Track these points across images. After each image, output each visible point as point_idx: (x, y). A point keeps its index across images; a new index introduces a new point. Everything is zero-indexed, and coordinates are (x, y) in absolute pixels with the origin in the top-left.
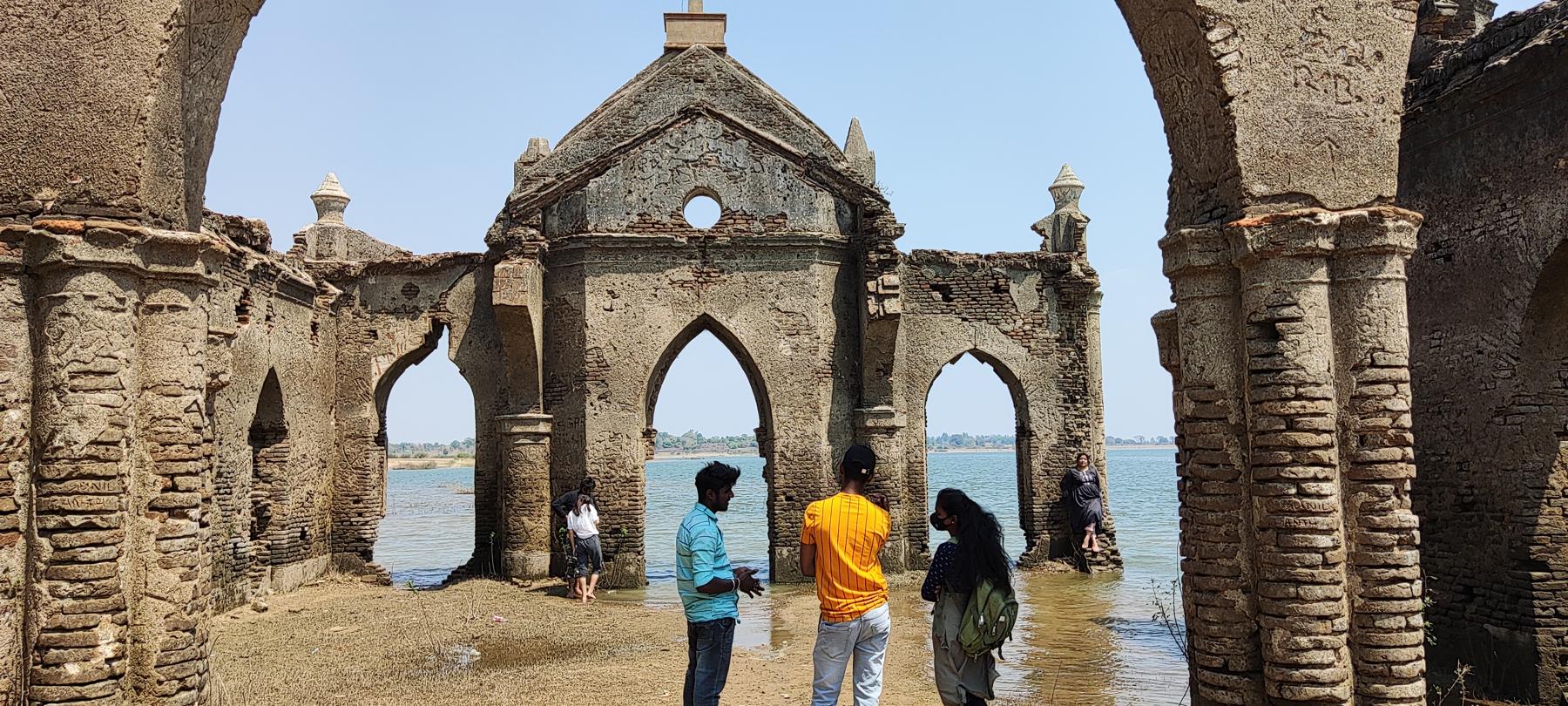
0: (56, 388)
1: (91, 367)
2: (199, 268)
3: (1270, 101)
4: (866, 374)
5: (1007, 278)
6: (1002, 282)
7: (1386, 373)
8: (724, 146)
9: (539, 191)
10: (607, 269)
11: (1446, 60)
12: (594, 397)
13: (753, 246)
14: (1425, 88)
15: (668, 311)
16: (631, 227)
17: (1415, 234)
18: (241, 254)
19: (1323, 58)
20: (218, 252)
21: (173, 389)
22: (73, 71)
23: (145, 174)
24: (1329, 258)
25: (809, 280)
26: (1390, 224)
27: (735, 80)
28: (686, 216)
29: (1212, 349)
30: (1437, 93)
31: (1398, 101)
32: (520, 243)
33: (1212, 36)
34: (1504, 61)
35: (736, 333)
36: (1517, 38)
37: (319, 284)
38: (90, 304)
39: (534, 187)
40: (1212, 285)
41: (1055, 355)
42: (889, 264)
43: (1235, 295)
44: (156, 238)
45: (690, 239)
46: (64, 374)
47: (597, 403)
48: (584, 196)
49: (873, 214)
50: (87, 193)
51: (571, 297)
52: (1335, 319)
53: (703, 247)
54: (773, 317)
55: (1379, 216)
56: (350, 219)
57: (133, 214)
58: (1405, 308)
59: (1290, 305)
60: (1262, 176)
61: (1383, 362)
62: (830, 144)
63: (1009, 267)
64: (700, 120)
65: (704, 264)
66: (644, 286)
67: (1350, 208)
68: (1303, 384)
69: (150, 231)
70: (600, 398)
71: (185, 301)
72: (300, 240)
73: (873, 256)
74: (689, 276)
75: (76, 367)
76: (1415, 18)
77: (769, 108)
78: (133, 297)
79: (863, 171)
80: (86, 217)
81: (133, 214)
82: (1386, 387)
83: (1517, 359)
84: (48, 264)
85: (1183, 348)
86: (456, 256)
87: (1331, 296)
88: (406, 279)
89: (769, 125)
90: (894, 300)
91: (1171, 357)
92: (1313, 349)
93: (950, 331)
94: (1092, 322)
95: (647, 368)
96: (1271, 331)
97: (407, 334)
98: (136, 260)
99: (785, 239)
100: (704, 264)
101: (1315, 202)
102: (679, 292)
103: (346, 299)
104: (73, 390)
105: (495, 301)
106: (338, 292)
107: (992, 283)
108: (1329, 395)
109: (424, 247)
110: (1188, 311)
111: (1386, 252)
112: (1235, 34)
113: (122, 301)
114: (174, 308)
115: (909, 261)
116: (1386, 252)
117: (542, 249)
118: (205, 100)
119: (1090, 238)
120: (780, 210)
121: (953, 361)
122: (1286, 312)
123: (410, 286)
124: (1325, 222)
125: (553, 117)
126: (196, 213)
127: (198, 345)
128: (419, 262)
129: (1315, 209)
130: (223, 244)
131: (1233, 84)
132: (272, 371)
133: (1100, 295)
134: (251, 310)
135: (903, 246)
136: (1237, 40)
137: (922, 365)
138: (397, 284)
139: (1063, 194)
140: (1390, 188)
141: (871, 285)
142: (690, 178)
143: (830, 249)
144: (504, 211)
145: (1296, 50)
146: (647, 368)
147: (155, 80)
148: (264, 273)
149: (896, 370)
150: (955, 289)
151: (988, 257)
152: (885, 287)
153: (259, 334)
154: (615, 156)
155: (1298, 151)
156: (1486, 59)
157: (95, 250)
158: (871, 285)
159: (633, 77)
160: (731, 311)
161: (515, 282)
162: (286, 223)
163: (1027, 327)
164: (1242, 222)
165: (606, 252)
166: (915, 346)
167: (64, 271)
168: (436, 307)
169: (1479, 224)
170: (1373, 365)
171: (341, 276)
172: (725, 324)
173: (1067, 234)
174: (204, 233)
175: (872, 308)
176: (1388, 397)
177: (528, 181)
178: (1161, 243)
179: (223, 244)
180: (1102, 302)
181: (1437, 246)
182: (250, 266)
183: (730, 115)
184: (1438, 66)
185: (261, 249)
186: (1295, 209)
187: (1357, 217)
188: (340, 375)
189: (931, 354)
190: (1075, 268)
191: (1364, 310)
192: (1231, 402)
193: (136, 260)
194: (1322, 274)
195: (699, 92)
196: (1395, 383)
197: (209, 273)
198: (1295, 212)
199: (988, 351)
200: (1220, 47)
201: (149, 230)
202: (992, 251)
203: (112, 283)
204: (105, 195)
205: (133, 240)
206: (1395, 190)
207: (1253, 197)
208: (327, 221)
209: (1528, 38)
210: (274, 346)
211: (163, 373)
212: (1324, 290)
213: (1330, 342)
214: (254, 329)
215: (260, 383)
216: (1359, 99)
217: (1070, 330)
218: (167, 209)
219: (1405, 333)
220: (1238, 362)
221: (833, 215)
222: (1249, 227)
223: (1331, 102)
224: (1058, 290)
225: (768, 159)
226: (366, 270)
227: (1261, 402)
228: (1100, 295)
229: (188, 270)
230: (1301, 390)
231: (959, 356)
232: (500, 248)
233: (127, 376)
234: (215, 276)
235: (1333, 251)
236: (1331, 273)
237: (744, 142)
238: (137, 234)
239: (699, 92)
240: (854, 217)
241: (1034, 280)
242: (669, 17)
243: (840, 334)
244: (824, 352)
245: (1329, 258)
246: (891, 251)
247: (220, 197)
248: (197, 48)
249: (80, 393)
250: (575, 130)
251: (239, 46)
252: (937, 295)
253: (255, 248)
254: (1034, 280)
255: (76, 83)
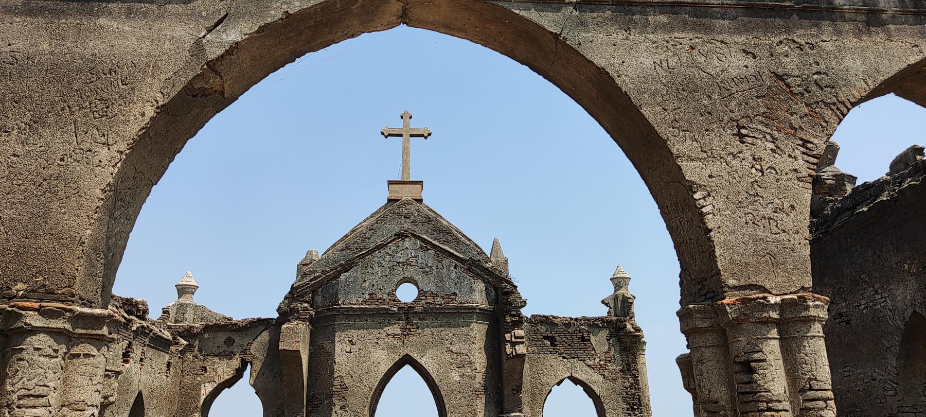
0: (8, 406)
1: (32, 392)
2: (105, 331)
3: (732, 232)
4: (505, 392)
5: (589, 332)
6: (585, 334)
7: (819, 394)
8: (420, 254)
9: (311, 281)
10: (349, 327)
11: (832, 209)
12: (337, 408)
13: (437, 313)
14: (822, 224)
15: (385, 353)
16: (364, 302)
17: (826, 309)
18: (130, 321)
19: (761, 209)
20: (118, 322)
21: (80, 406)
22: (45, 216)
23: (80, 275)
24: (778, 323)
25: (470, 333)
26: (811, 304)
27: (427, 217)
28: (397, 295)
29: (714, 379)
30: (829, 227)
31: (807, 233)
32: (298, 311)
33: (697, 196)
34: (865, 209)
35: (426, 366)
36: (871, 196)
37: (174, 338)
38: (37, 353)
39: (308, 278)
40: (710, 339)
41: (620, 380)
42: (518, 323)
43: (724, 346)
44: (81, 313)
45: (399, 309)
46: (15, 397)
47: (339, 412)
48: (338, 283)
49: (508, 294)
50: (44, 286)
51: (327, 345)
52: (785, 360)
53: (407, 313)
54: (448, 356)
55: (803, 299)
56: (197, 299)
57: (70, 298)
58: (825, 354)
59: (758, 352)
60: (733, 275)
61: (817, 387)
62: (482, 252)
63: (590, 326)
64: (407, 239)
65: (407, 323)
66: (371, 337)
67: (786, 294)
68: (771, 401)
69: (78, 309)
70: (341, 409)
71: (94, 351)
72: (166, 311)
73: (508, 318)
74: (398, 331)
75: (23, 392)
76: (811, 186)
77: (447, 233)
78: (63, 349)
79: (501, 268)
80: (42, 300)
81: (70, 298)
82: (820, 402)
83: (897, 384)
84: (15, 328)
85: (697, 378)
86: (259, 320)
87: (781, 346)
88: (228, 334)
89: (446, 242)
90: (521, 346)
91: (690, 383)
92: (774, 379)
93: (556, 365)
94: (641, 360)
95: (371, 389)
96: (749, 368)
97: (224, 369)
98: (68, 326)
99: (456, 308)
100: (407, 323)
101: (765, 290)
102: (392, 341)
103: (190, 347)
104: (19, 407)
105: (280, 348)
106: (185, 343)
107: (580, 335)
108: (788, 408)
109: (239, 315)
110: (697, 355)
111: (811, 320)
112: (709, 195)
113: (56, 351)
114: (87, 356)
115: (530, 321)
116: (811, 320)
117: (311, 315)
118: (120, 232)
119: (636, 308)
120: (453, 290)
121: (558, 384)
122: (756, 356)
123: (230, 338)
124: (772, 302)
125: (322, 238)
126: (107, 296)
127: (99, 378)
128: (236, 324)
129: (766, 295)
130: (120, 315)
131: (711, 223)
132: (140, 393)
133: (644, 343)
134: (132, 355)
135: (526, 312)
136: (711, 199)
137: (539, 386)
138: (222, 337)
139: (619, 282)
140: (809, 283)
141: (507, 336)
142: (400, 272)
143: (482, 314)
144: (290, 293)
145: (745, 204)
146: (371, 389)
147: (92, 221)
148: (142, 332)
149: (524, 390)
150: (558, 338)
151: (576, 319)
152: (516, 338)
153: (134, 370)
154: (357, 260)
155: (751, 260)
156: (854, 208)
157: (44, 320)
158: (507, 336)
159: (369, 215)
160: (423, 353)
161: (293, 336)
162: (158, 301)
163: (602, 363)
164: (725, 301)
165: (349, 317)
166: (535, 373)
167: (24, 333)
168: (244, 352)
169: (864, 302)
170: (811, 389)
171: (188, 333)
172: (419, 360)
173: (622, 306)
174: (110, 310)
175: (509, 351)
176: (822, 409)
177: (305, 275)
178: (678, 313)
179: (120, 315)
180: (646, 347)
181: (841, 315)
182: (134, 328)
183: (424, 237)
184: (828, 211)
185: (142, 318)
186: (754, 294)
187: (792, 299)
188: (181, 396)
189: (545, 379)
190: (629, 326)
191: (802, 355)
192: (729, 413)
193: (68, 326)
194: (774, 333)
195: (407, 224)
196: (826, 400)
197: (110, 334)
198: (754, 296)
199: (579, 377)
200: (701, 202)
201: (78, 308)
202: (579, 316)
203: (52, 340)
204: (55, 287)
205: (68, 314)
206: (811, 283)
207: (729, 287)
208: (183, 300)
209: (877, 196)
210: (143, 378)
211: (76, 395)
212: (776, 343)
213: (784, 374)
214: (132, 367)
215: (132, 400)
216: (784, 232)
217: (628, 365)
218: (90, 296)
219: (827, 369)
220: (730, 387)
221: (484, 294)
222: (728, 304)
223: (768, 233)
224: (619, 340)
225: (446, 262)
226: (203, 329)
227: (747, 413)
228: (644, 343)
229: (98, 332)
230: (770, 405)
231: (562, 381)
232: (285, 314)
233: (53, 398)
234: (114, 336)
235: (780, 320)
236: (779, 332)
237: (432, 252)
238: (70, 311)
239: (407, 224)
240: (497, 295)
241: (604, 334)
242: (390, 183)
243: (489, 367)
244: (480, 378)
245: (778, 323)
246: (519, 315)
247: (121, 288)
248: (119, 203)
249: (23, 409)
250: (334, 245)
251: (144, 201)
252: (548, 343)
253: (138, 317)
254: (604, 334)
255: (46, 223)
